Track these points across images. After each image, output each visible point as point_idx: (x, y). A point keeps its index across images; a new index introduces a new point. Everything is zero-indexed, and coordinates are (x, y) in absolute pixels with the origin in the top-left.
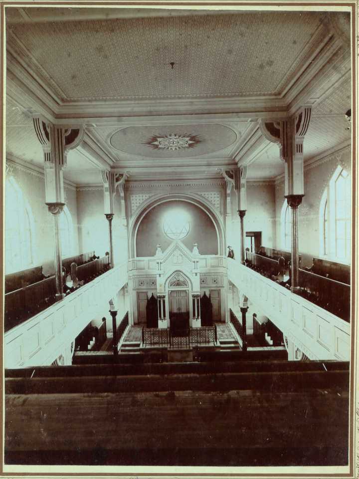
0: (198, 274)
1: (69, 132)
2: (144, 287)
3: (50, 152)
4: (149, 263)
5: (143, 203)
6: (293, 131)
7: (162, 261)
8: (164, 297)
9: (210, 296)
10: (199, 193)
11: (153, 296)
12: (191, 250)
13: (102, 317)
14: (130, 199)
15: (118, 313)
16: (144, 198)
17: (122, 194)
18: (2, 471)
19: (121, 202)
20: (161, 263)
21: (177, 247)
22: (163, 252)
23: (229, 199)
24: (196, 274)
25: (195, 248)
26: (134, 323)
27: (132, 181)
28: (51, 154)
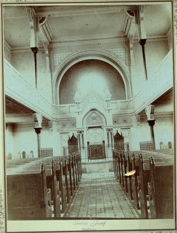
1: (41, 18)
4: (69, 109)
6: (139, 11)
9: (121, 134)
10: (109, 50)
13: (31, 151)
14: (53, 57)
16: (65, 56)
17: (47, 52)
19: (45, 59)
23: (132, 52)
27: (57, 42)
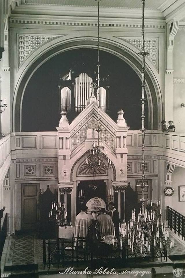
0: (125, 156)
2: (32, 178)
3: (173, 40)
5: (38, 48)
7: (68, 135)
8: (70, 190)
11: (48, 188)
12: (115, 118)
15: (6, 208)
18: (86, 205)
20: (66, 138)
21: (93, 113)
22: (70, 123)
24: (122, 155)
25: (121, 117)
26: (16, 231)
28: (173, 41)
